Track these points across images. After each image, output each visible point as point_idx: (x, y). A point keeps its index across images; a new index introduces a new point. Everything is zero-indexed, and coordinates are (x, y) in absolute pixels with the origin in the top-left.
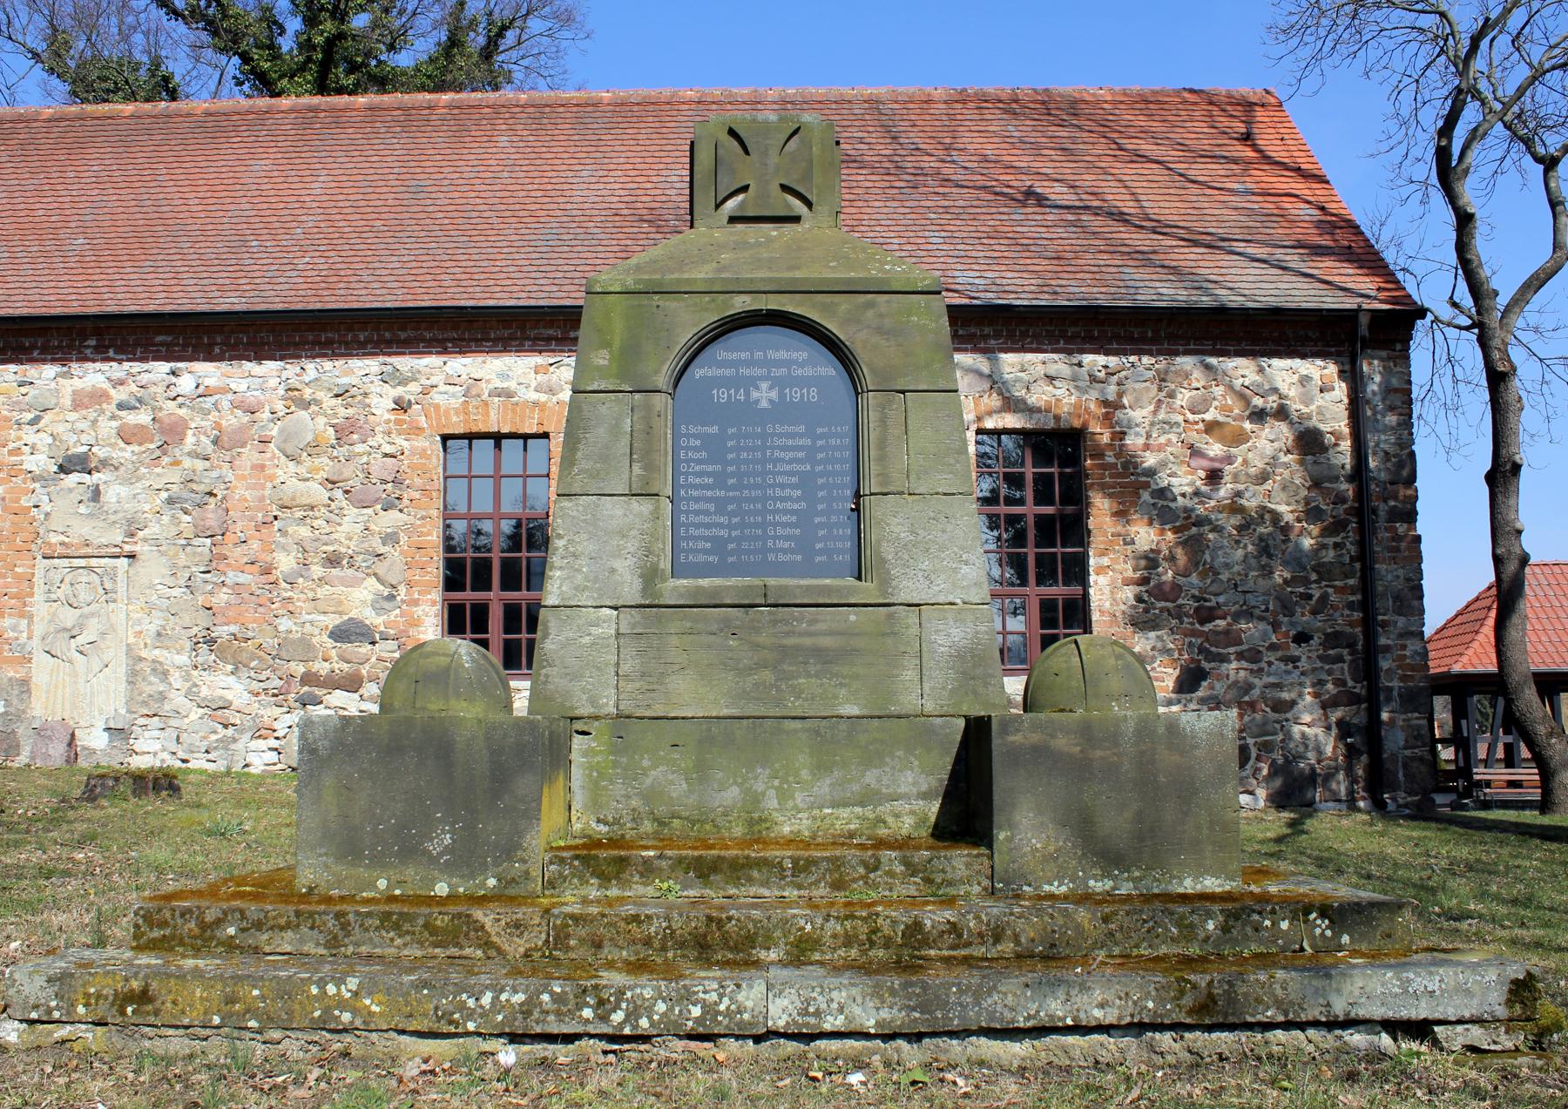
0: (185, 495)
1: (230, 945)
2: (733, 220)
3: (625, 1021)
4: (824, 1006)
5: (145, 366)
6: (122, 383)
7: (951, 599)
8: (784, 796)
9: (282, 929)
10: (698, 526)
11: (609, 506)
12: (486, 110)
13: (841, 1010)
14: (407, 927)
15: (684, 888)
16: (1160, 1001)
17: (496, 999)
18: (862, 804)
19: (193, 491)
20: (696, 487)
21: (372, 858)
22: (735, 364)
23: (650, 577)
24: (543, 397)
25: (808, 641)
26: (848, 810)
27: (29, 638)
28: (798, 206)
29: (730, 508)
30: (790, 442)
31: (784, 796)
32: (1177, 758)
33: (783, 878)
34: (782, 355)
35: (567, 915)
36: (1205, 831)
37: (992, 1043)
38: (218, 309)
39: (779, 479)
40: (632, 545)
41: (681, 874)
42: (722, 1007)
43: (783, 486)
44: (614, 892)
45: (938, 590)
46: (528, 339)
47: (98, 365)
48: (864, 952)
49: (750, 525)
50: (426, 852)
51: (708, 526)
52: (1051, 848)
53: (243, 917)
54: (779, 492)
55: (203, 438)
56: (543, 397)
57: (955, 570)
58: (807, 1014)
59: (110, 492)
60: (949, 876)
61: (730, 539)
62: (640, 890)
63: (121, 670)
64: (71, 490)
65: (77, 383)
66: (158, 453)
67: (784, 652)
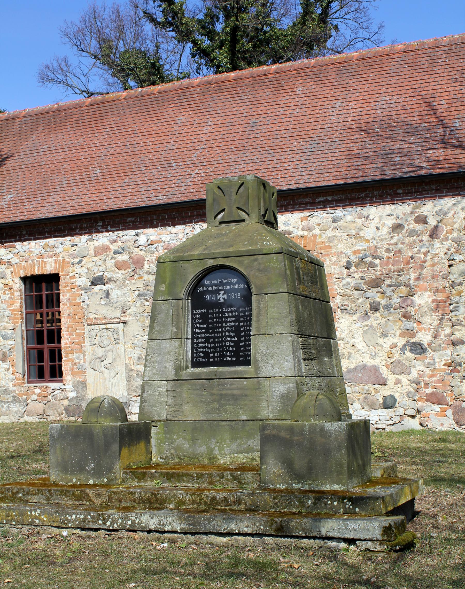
0: (146, 292)
1: (20, 500)
2: (221, 223)
3: (110, 525)
4: (165, 522)
5: (124, 233)
6: (115, 241)
7: (280, 375)
8: (221, 449)
9: (34, 495)
10: (200, 348)
11: (165, 343)
12: (294, 72)
13: (170, 524)
14: (68, 494)
15: (163, 483)
16: (265, 526)
17: (76, 517)
18: (247, 453)
19: (149, 290)
20: (199, 333)
21: (71, 472)
22: (212, 286)
23: (178, 369)
24: (305, 233)
25: (229, 392)
26: (243, 455)
27: (85, 362)
28: (243, 215)
29: (211, 340)
30: (231, 315)
31: (221, 449)
32: (324, 440)
33: (194, 480)
34: (228, 281)
35: (111, 492)
36: (334, 467)
37: (216, 537)
38: (153, 203)
39: (228, 329)
40: (172, 358)
41: (162, 478)
42: (137, 522)
43: (229, 332)
44: (142, 484)
45: (276, 372)
46: (297, 204)
47: (104, 234)
48: (198, 506)
49: (218, 347)
50: (86, 470)
51: (203, 348)
52: (280, 472)
53: (24, 491)
54: (227, 334)
55: (152, 265)
56: (305, 233)
57: (282, 364)
58: (160, 525)
59: (114, 293)
60: (246, 481)
61: (211, 353)
62: (150, 483)
63: (123, 375)
64: (97, 293)
65: (96, 243)
66: (133, 273)
67: (222, 396)
